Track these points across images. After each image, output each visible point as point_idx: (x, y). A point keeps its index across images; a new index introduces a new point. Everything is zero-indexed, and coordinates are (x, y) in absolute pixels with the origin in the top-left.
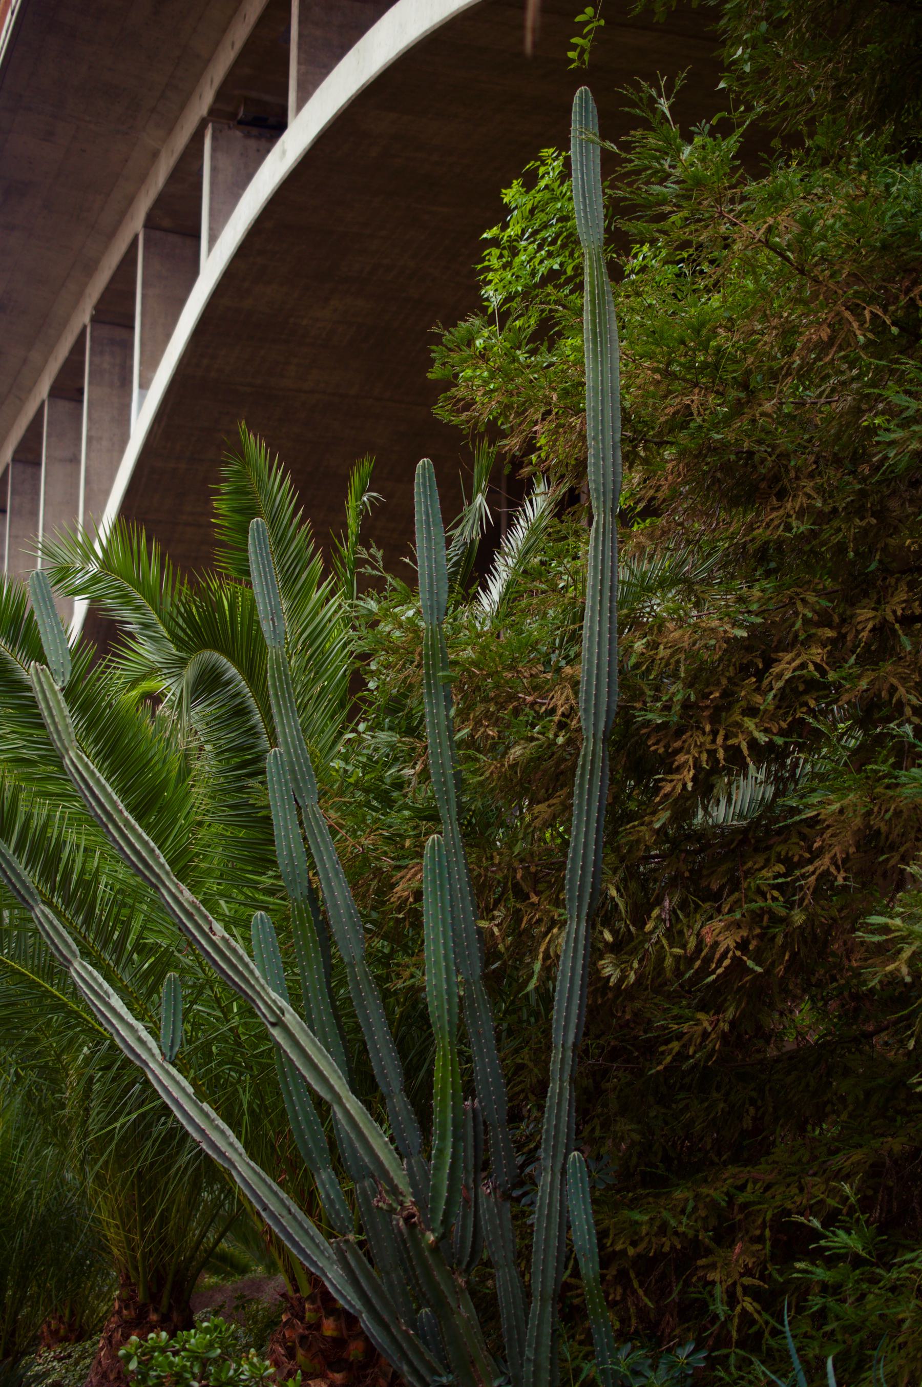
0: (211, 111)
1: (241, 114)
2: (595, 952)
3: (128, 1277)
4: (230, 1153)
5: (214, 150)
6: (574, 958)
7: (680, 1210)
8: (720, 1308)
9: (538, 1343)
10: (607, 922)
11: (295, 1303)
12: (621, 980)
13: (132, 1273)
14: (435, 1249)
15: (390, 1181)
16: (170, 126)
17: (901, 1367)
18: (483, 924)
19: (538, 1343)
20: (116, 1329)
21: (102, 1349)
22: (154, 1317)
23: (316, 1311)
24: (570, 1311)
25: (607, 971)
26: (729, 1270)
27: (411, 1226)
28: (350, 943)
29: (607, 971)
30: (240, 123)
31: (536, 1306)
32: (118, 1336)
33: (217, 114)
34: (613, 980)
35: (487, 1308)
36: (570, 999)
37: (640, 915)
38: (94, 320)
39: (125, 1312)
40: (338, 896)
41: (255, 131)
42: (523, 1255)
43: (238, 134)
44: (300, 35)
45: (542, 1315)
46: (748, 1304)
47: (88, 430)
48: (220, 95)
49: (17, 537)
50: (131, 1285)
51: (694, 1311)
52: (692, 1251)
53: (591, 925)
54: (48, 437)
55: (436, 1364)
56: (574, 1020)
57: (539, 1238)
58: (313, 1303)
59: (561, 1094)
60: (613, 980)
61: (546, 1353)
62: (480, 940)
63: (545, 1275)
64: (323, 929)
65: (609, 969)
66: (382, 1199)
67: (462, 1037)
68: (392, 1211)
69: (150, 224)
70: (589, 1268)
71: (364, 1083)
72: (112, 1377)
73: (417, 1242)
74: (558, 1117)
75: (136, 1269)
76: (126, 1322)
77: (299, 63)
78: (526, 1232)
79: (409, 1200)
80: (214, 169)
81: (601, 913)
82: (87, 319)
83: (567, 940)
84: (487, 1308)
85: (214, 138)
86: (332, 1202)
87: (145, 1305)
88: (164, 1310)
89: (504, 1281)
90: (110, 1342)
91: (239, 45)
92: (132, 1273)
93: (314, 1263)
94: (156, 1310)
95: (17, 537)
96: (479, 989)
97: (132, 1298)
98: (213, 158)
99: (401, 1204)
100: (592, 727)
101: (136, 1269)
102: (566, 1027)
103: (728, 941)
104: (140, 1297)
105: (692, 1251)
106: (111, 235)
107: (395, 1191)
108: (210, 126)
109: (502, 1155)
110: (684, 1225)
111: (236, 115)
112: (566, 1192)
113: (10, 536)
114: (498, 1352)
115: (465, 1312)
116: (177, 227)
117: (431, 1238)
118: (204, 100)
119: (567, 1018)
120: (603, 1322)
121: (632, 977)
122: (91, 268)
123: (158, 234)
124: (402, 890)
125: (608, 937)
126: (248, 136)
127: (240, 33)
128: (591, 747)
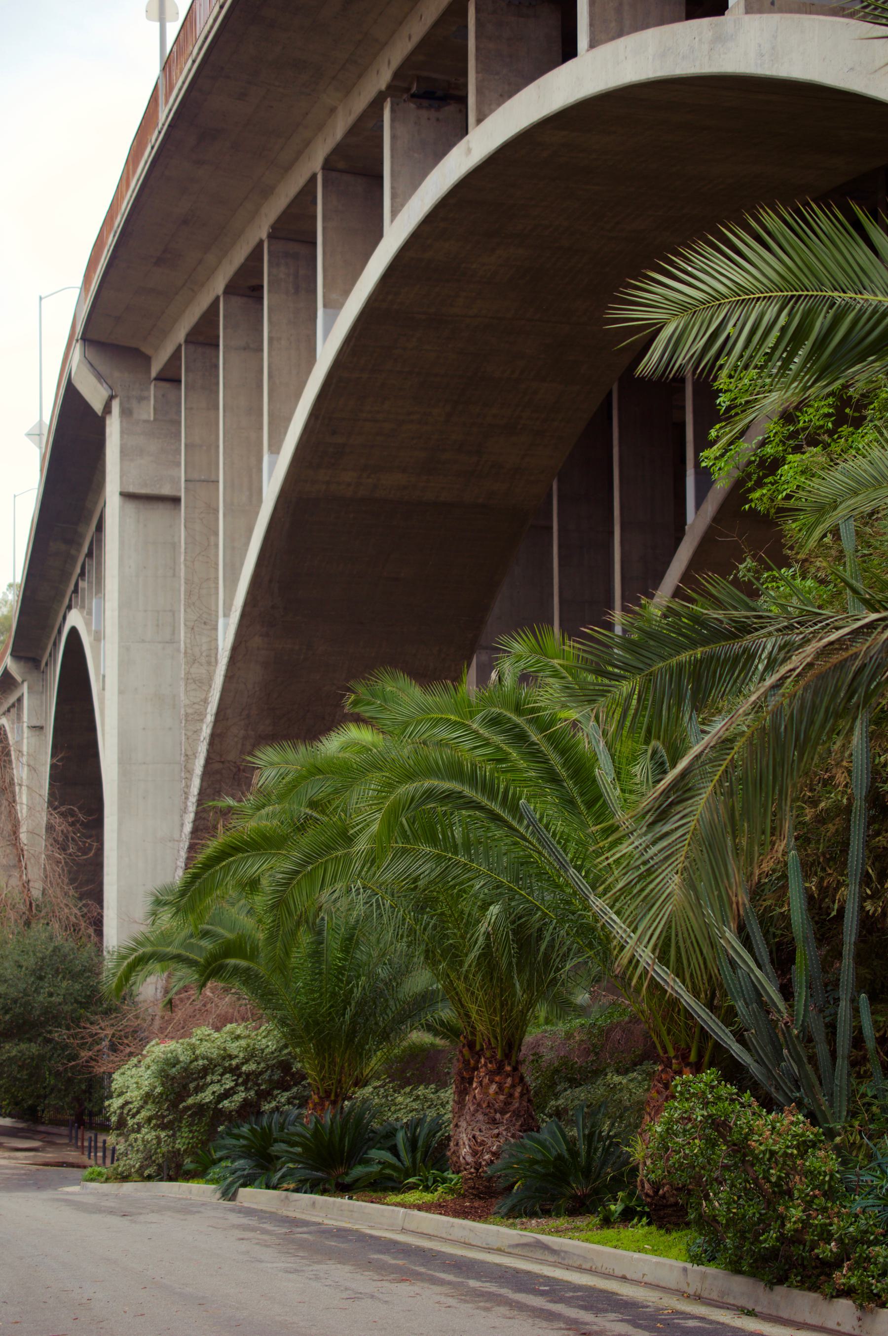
0: (389, 87)
1: (414, 89)
2: (864, 898)
3: (490, 1044)
4: (680, 991)
5: (393, 120)
6: (854, 903)
9: (841, 1078)
10: (868, 886)
11: (665, 1059)
12: (876, 910)
13: (492, 1040)
14: (797, 1037)
15: (777, 1007)
16: (348, 90)
17: (780, 1148)
18: (807, 885)
19: (841, 1078)
20: (484, 1076)
21: (476, 1088)
23: (679, 1064)
25: (868, 908)
27: (788, 1027)
29: (868, 908)
30: (413, 96)
31: (839, 1061)
32: (486, 1080)
33: (396, 89)
34: (871, 912)
36: (852, 922)
38: (270, 236)
39: (489, 1065)
41: (425, 103)
43: (412, 106)
44: (478, 49)
47: (270, 332)
48: (396, 75)
49: (191, 409)
50: (492, 1048)
53: (860, 886)
54: (224, 329)
55: (792, 1088)
56: (854, 931)
58: (677, 1059)
59: (849, 965)
60: (871, 912)
61: (845, 1082)
62: (806, 893)
65: (869, 906)
66: (773, 1015)
68: (779, 1020)
69: (328, 166)
72: (484, 1106)
73: (790, 1034)
74: (848, 976)
75: (496, 1038)
76: (491, 1071)
77: (477, 72)
79: (785, 1015)
80: (393, 137)
81: (866, 879)
82: (264, 233)
85: (393, 111)
86: (744, 1016)
87: (502, 1061)
88: (514, 1064)
90: (481, 1085)
91: (416, 39)
92: (492, 1040)
93: (725, 1042)
94: (509, 1064)
95: (191, 409)
97: (493, 1057)
98: (392, 127)
99: (782, 1017)
100: (860, 792)
101: (496, 1038)
102: (850, 935)
106: (288, 168)
107: (779, 1011)
108: (389, 100)
111: (409, 89)
113: (186, 409)
116: (358, 174)
117: (796, 1032)
118: (382, 77)
119: (851, 931)
120: (874, 1067)
121: (879, 909)
122: (267, 192)
125: (869, 892)
126: (420, 107)
127: (417, 29)
128: (859, 804)
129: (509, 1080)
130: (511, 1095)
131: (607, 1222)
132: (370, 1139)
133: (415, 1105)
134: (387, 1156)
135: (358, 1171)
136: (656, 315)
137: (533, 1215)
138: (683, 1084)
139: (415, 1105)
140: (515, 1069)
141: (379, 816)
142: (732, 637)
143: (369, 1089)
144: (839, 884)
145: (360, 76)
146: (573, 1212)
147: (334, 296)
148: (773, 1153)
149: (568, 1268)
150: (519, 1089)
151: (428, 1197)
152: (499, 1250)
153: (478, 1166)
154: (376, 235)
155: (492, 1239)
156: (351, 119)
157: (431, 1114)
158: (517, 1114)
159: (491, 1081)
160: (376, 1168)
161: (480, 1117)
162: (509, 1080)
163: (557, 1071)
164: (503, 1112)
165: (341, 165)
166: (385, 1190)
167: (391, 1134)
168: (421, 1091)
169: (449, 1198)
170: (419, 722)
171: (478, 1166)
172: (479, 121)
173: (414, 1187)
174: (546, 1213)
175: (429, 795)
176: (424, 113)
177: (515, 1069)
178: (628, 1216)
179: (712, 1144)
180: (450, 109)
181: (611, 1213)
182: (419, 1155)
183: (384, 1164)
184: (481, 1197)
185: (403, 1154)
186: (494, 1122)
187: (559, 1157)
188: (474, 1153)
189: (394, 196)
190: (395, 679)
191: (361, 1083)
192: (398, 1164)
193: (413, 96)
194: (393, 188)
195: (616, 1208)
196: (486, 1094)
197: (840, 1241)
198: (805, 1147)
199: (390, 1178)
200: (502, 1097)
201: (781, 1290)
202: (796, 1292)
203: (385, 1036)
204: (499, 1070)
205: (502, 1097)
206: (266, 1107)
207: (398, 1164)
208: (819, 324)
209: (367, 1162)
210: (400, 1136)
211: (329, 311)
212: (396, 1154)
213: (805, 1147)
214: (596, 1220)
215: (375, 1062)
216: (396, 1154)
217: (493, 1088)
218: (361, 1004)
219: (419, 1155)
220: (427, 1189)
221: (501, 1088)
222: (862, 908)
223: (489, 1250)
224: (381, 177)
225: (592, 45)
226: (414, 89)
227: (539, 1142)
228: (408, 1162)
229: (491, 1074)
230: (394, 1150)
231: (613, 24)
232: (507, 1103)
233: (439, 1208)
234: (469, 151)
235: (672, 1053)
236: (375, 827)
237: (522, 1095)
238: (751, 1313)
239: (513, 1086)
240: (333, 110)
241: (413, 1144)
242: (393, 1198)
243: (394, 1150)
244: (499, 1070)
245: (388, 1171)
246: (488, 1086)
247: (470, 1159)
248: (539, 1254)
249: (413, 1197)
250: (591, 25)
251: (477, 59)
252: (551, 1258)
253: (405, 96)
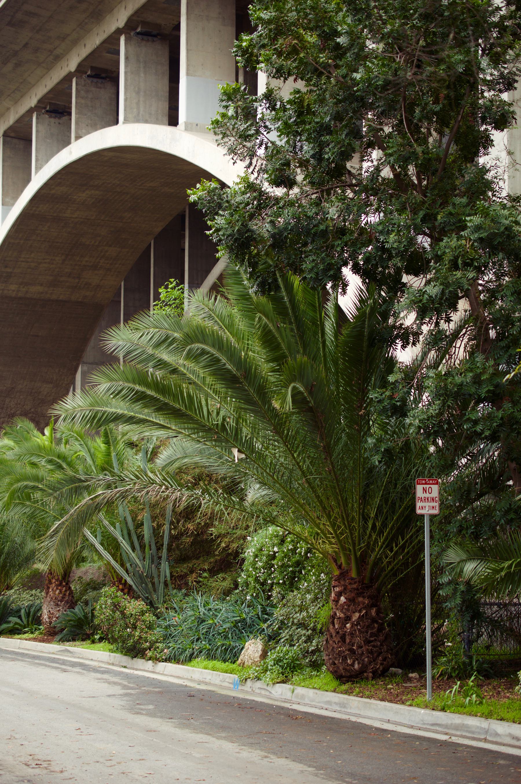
0: (36, 106)
2: (170, 529)
5: (37, 123)
7: (183, 568)
8: (190, 584)
22: (64, 584)
24: (166, 584)
26: (191, 579)
28: (131, 527)
32: (55, 588)
35: (153, 584)
37: (178, 523)
40: (129, 519)
41: (53, 115)
42: (159, 576)
43: (47, 116)
44: (76, 103)
45: (162, 585)
46: (195, 583)
48: (39, 101)
51: (186, 584)
52: (186, 575)
57: (161, 574)
63: (162, 580)
64: (127, 523)
67: (150, 546)
70: (169, 579)
71: (133, 549)
77: (76, 114)
78: (160, 572)
80: (37, 131)
81: (172, 523)
83: (166, 527)
84: (153, 584)
85: (37, 118)
89: (156, 580)
96: (152, 535)
98: (37, 127)
103: (192, 528)
104: (60, 579)
105: (186, 575)
109: (156, 560)
110: (185, 571)
112: (165, 568)
114: (155, 590)
115: (150, 585)
123: (9, 139)
124: (139, 518)
129: (64, 588)
130: (65, 595)
131: (93, 642)
132: (10, 613)
133: (31, 598)
134: (18, 621)
135: (4, 626)
136: (60, 413)
137: (69, 641)
138: (105, 592)
139: (31, 598)
140: (67, 584)
141: (7, 495)
142: (84, 481)
143: (13, 591)
144: (164, 524)
145: (22, 97)
146: (83, 640)
147: (7, 200)
148: (132, 615)
149: (75, 657)
150: (68, 592)
151: (31, 636)
152: (53, 653)
153: (51, 623)
154: (28, 180)
155: (52, 648)
156: (17, 116)
157: (38, 602)
158: (67, 602)
159: (57, 589)
160: (11, 625)
161: (52, 603)
162: (64, 588)
163: (88, 584)
164: (61, 601)
165: (12, 134)
166: (14, 634)
167: (19, 611)
168: (34, 592)
169: (40, 636)
170: (25, 455)
171: (51, 623)
172: (78, 138)
173: (25, 633)
174: (74, 640)
175: (26, 487)
176: (52, 120)
177: (67, 584)
178: (101, 640)
179: (114, 612)
180: (65, 118)
181: (95, 639)
182: (30, 619)
183: (16, 623)
184: (52, 634)
185: (23, 618)
186: (57, 605)
187: (80, 619)
188: (49, 618)
189: (37, 160)
190: (23, 421)
191: (9, 588)
192: (21, 623)
193: (47, 111)
194: (36, 156)
195: (97, 637)
196: (55, 594)
197: (150, 642)
198: (143, 613)
199: (17, 629)
200: (61, 595)
201: (135, 659)
202: (139, 660)
203: (20, 566)
204: (60, 584)
205: (61, 595)
206: (466, 287)
207: (21, 623)
208: (99, 415)
209: (9, 622)
210: (23, 611)
211: (5, 207)
212: (21, 620)
213: (143, 613)
214: (89, 642)
215: (16, 578)
216: (21, 620)
217: (58, 591)
218: (8, 554)
219: (30, 619)
220: (32, 633)
221: (61, 592)
222: (170, 532)
223: (50, 653)
224: (31, 141)
225: (124, 123)
226: (48, 108)
227: (73, 613)
228: (25, 622)
229: (57, 586)
230: (20, 617)
231: (135, 110)
232: (63, 598)
233: (35, 639)
234: (71, 153)
235: (116, 580)
236: (6, 499)
237: (69, 594)
238: (125, 667)
239: (66, 591)
240: (8, 109)
241: (28, 614)
242: (17, 636)
243: (20, 617)
244: (60, 584)
245: (17, 626)
246: (56, 591)
247: (47, 620)
248: (66, 654)
249: (26, 636)
250: (125, 110)
251: (76, 108)
252: (70, 655)
253: (43, 111)
